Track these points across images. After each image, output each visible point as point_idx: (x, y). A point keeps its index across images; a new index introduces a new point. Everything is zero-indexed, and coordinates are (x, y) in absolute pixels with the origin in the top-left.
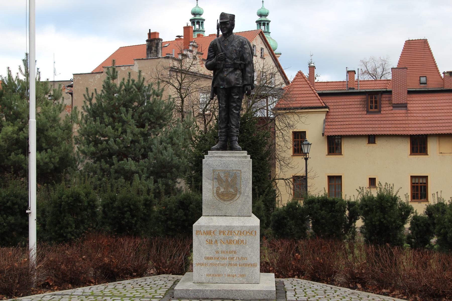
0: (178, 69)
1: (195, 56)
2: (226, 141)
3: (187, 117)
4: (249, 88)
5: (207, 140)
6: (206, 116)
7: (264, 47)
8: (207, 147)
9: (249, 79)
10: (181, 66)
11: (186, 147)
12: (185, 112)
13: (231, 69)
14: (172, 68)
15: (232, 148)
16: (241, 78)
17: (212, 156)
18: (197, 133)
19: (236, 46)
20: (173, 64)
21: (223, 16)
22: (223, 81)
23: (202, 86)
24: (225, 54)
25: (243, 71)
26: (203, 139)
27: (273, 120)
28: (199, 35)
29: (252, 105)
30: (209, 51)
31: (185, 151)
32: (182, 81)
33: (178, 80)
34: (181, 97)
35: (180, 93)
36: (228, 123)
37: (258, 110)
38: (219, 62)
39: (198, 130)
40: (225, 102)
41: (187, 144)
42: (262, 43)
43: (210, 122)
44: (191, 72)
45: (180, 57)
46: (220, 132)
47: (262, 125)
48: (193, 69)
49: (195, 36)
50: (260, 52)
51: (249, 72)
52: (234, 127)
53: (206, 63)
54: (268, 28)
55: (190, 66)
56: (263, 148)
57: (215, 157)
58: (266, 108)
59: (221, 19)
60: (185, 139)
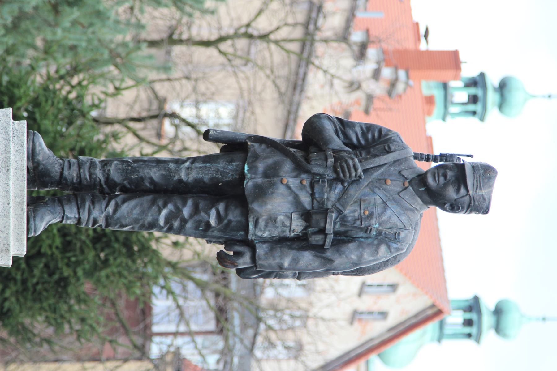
0: (317, 28)
1: (359, 87)
2: (62, 181)
3: (150, 57)
4: (245, 262)
5: (70, 123)
6: (155, 122)
7: (392, 320)
8: (47, 124)
9: (273, 262)
10: (326, 41)
11: (47, 52)
12: (168, 53)
13: (305, 199)
14: (320, 9)
15: (35, 203)
16: (276, 233)
17: (7, 133)
18: (94, 92)
19: (384, 218)
20: (334, 13)
21: (486, 173)
22: (266, 175)
23: (258, 110)
24: (357, 181)
25: (300, 242)
26: (74, 112)
27: (141, 352)
28: (430, 100)
29: (192, 279)
30: (369, 128)
31: (35, 48)
32: (277, 42)
33: (278, 28)
34: (222, 39)
35: (236, 35)
36: (124, 190)
37: (175, 300)
38: (331, 160)
39: (106, 94)
40: (198, 182)
41: (59, 55)
42: (404, 317)
43: (136, 135)
44: (305, 74)
45: (357, 37)
46: (93, 165)
47: (125, 314)
48: (315, 80)
49: (429, 87)
50: (376, 308)
51: (295, 261)
52: (110, 209)
53: (329, 118)
54: (455, 336)
55: (325, 72)
56: (41, 318)
57: (7, 146)
58: (182, 328)
59: (474, 167)
60: (73, 48)
